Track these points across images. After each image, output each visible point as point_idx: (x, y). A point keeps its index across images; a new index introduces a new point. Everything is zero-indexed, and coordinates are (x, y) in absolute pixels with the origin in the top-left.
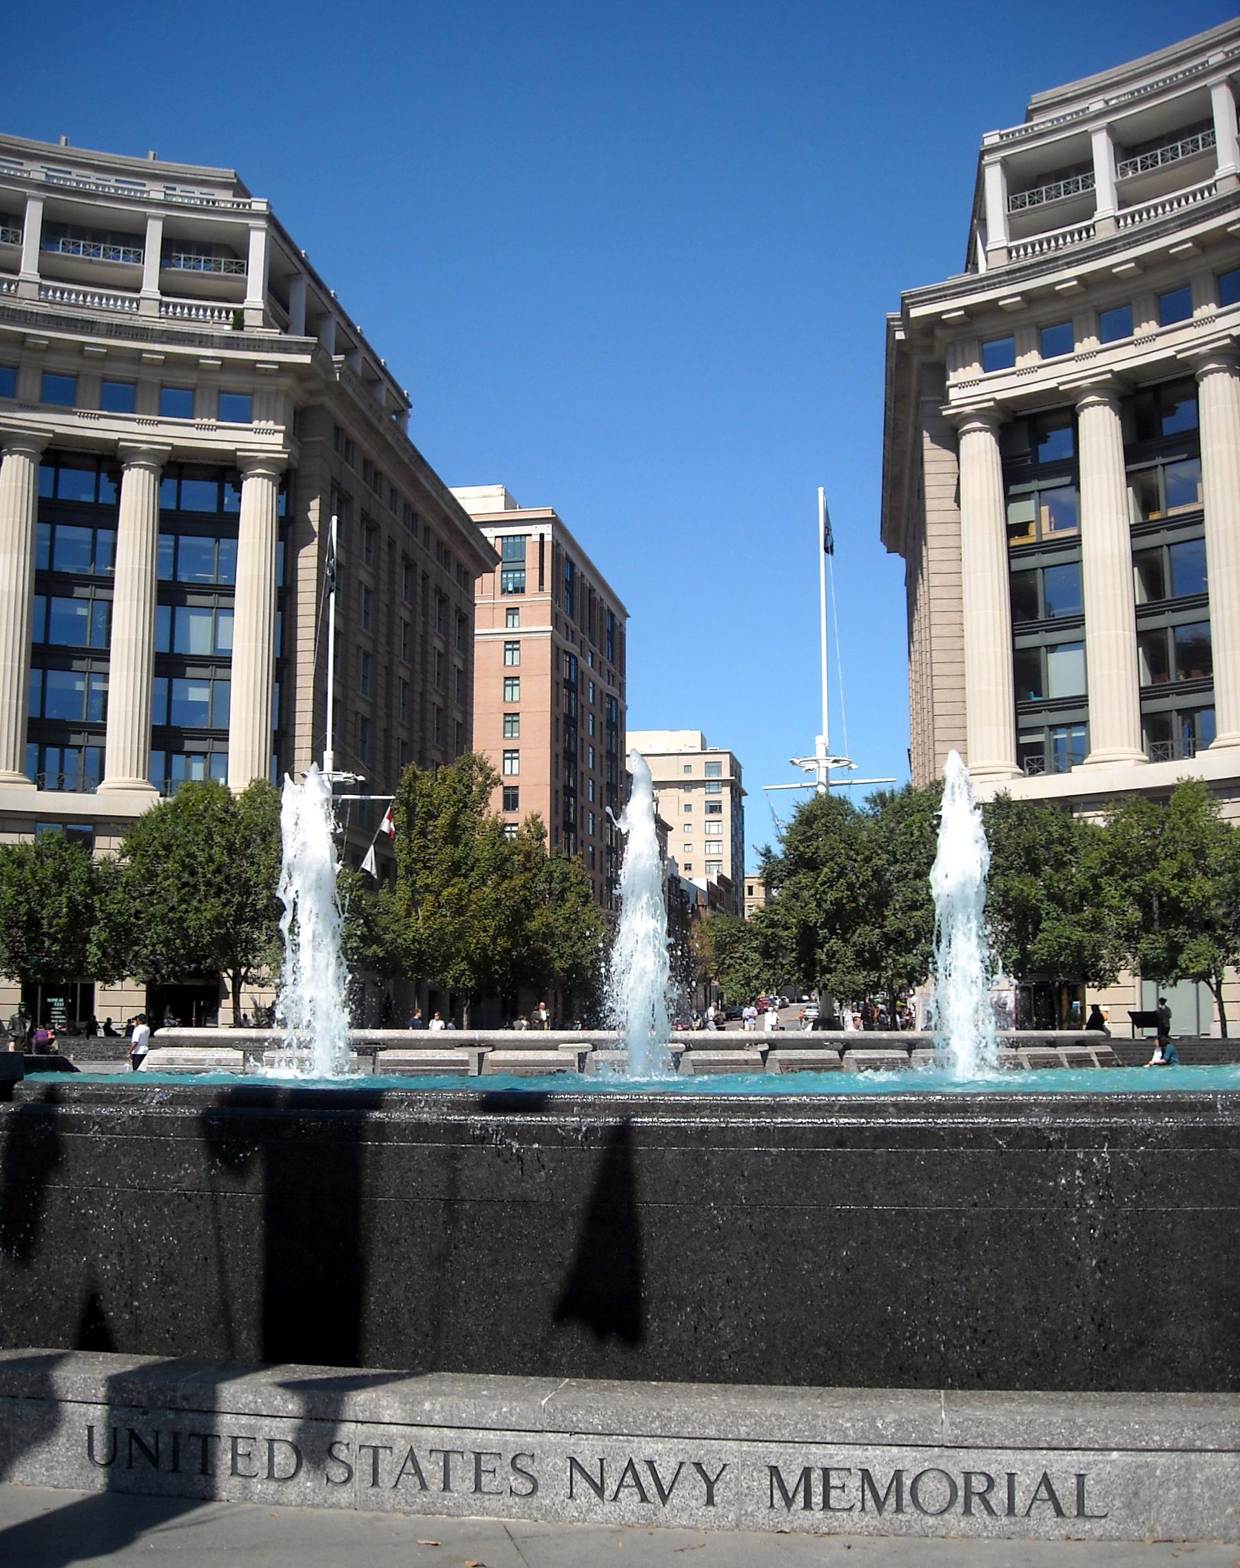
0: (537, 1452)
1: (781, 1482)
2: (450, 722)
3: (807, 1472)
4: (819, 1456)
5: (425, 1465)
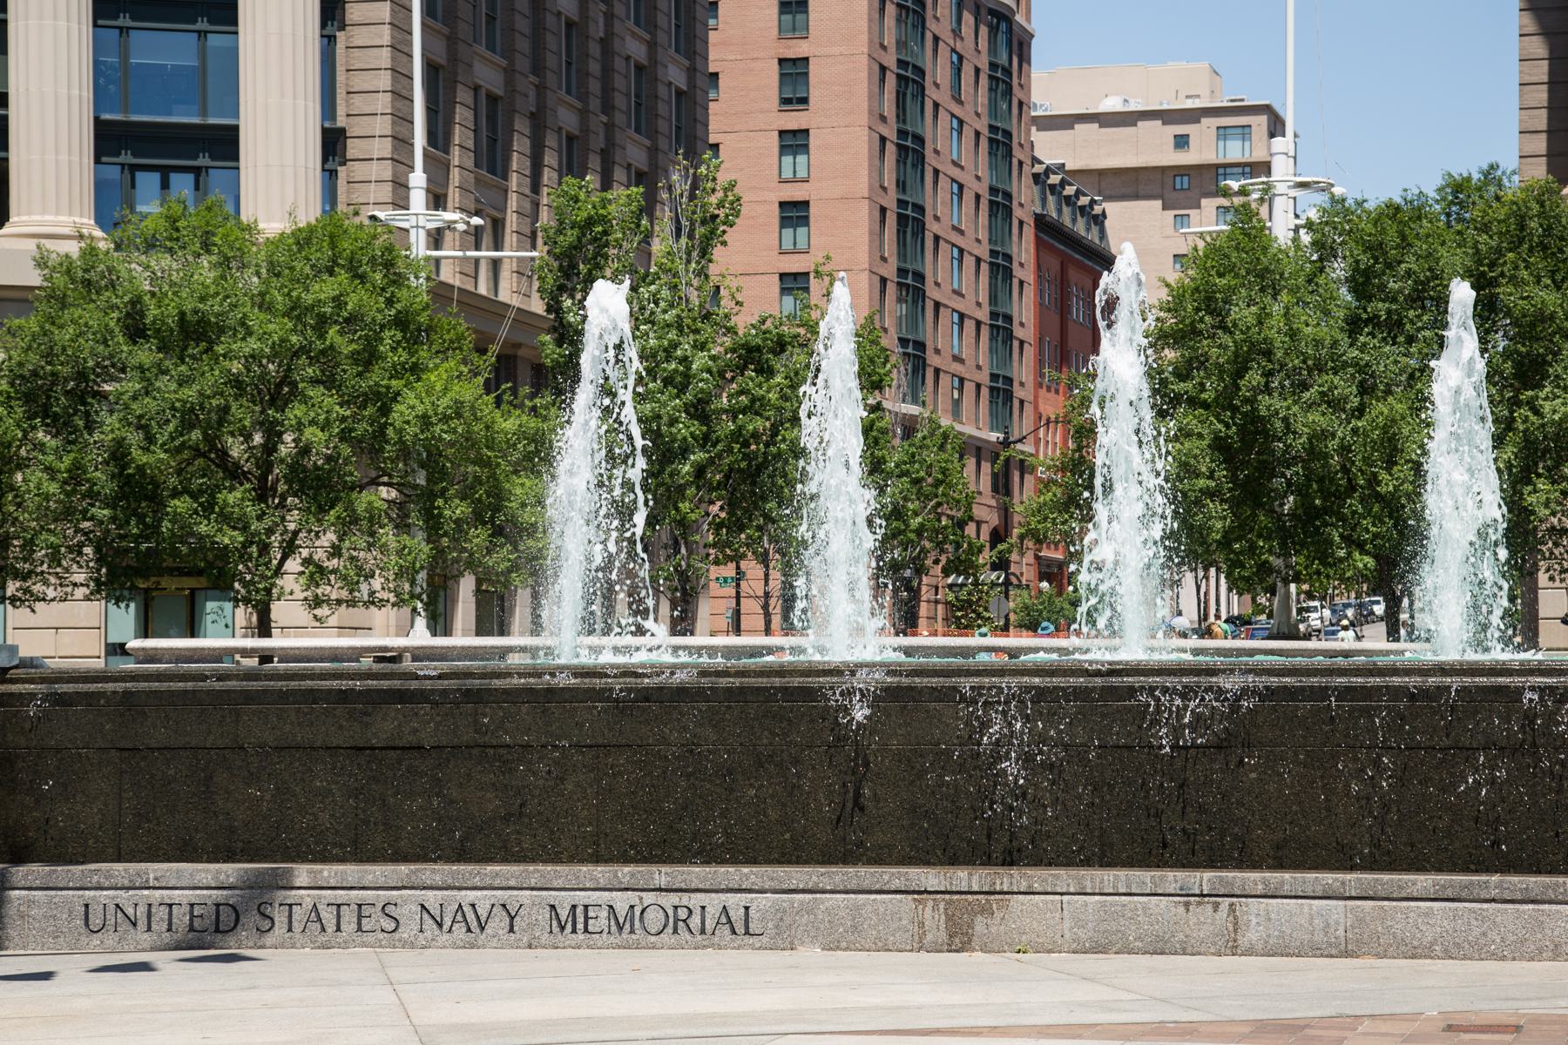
0: (399, 901)
1: (557, 914)
2: (662, 91)
3: (574, 907)
4: (581, 897)
5: (324, 915)
